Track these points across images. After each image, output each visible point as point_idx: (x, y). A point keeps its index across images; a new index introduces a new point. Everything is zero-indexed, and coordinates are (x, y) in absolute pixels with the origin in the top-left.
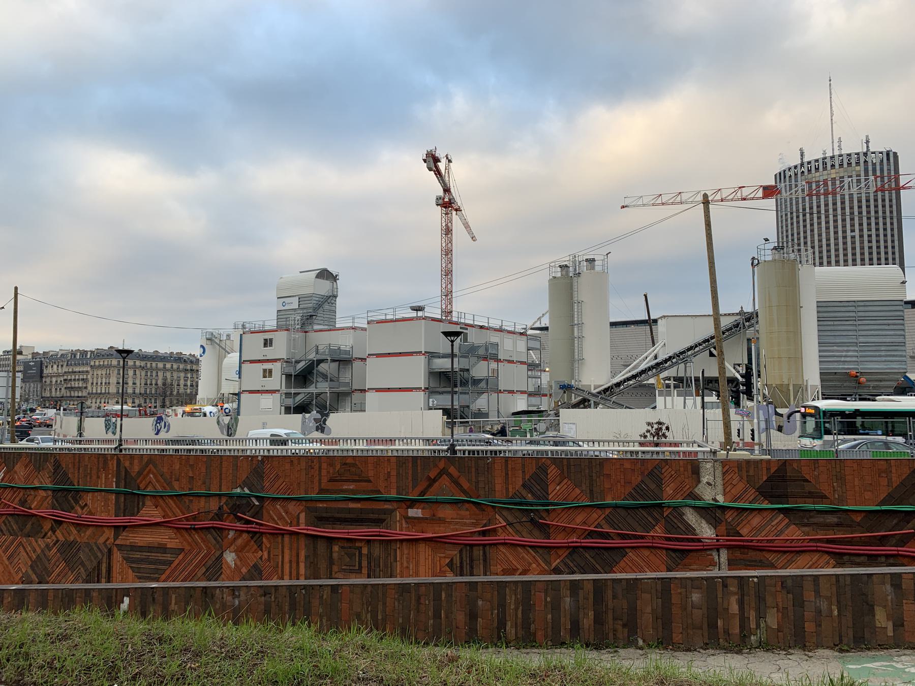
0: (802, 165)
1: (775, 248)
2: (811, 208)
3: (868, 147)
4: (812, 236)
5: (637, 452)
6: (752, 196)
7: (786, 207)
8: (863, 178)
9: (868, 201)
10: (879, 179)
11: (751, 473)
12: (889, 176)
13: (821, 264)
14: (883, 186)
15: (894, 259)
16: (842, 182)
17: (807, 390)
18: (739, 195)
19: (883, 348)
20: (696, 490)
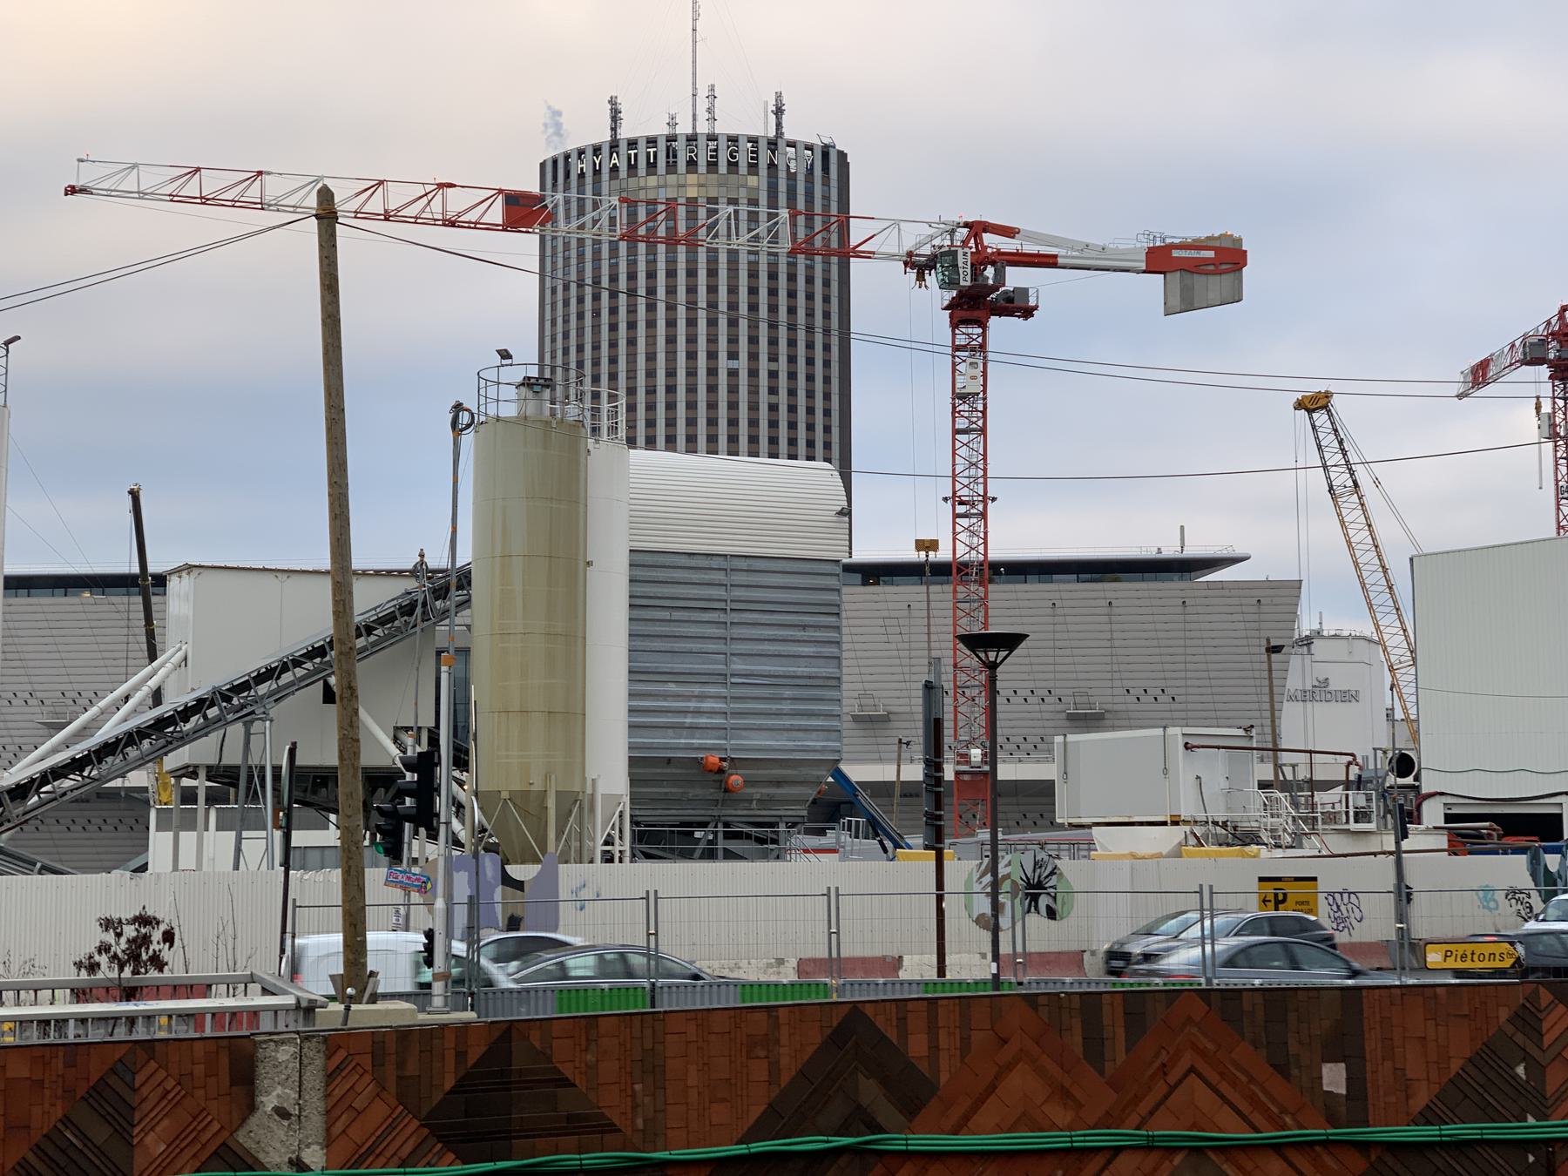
0: (614, 145)
1: (527, 383)
2: (614, 278)
3: (779, 125)
4: (632, 357)
5: (62, 1022)
6: (472, 216)
7: (567, 264)
8: (763, 209)
9: (773, 276)
10: (801, 220)
11: (412, 1068)
12: (826, 214)
13: (651, 443)
14: (810, 239)
15: (827, 445)
16: (712, 213)
17: (592, 809)
18: (436, 206)
19: (788, 693)
20: (241, 1137)
